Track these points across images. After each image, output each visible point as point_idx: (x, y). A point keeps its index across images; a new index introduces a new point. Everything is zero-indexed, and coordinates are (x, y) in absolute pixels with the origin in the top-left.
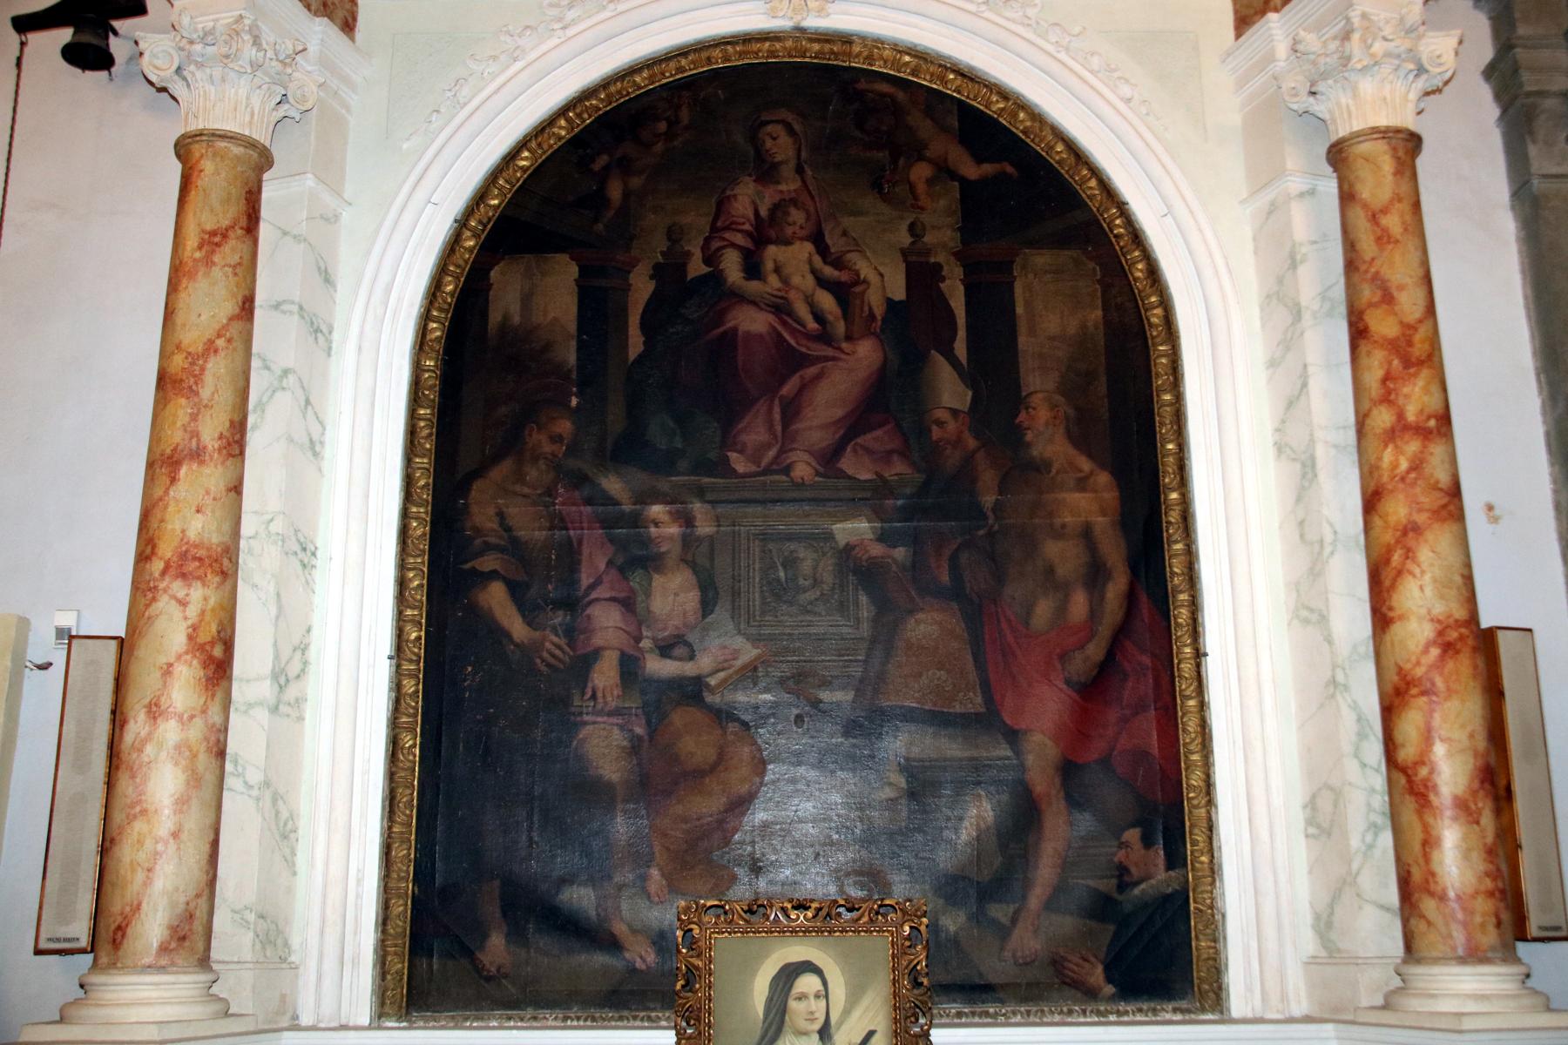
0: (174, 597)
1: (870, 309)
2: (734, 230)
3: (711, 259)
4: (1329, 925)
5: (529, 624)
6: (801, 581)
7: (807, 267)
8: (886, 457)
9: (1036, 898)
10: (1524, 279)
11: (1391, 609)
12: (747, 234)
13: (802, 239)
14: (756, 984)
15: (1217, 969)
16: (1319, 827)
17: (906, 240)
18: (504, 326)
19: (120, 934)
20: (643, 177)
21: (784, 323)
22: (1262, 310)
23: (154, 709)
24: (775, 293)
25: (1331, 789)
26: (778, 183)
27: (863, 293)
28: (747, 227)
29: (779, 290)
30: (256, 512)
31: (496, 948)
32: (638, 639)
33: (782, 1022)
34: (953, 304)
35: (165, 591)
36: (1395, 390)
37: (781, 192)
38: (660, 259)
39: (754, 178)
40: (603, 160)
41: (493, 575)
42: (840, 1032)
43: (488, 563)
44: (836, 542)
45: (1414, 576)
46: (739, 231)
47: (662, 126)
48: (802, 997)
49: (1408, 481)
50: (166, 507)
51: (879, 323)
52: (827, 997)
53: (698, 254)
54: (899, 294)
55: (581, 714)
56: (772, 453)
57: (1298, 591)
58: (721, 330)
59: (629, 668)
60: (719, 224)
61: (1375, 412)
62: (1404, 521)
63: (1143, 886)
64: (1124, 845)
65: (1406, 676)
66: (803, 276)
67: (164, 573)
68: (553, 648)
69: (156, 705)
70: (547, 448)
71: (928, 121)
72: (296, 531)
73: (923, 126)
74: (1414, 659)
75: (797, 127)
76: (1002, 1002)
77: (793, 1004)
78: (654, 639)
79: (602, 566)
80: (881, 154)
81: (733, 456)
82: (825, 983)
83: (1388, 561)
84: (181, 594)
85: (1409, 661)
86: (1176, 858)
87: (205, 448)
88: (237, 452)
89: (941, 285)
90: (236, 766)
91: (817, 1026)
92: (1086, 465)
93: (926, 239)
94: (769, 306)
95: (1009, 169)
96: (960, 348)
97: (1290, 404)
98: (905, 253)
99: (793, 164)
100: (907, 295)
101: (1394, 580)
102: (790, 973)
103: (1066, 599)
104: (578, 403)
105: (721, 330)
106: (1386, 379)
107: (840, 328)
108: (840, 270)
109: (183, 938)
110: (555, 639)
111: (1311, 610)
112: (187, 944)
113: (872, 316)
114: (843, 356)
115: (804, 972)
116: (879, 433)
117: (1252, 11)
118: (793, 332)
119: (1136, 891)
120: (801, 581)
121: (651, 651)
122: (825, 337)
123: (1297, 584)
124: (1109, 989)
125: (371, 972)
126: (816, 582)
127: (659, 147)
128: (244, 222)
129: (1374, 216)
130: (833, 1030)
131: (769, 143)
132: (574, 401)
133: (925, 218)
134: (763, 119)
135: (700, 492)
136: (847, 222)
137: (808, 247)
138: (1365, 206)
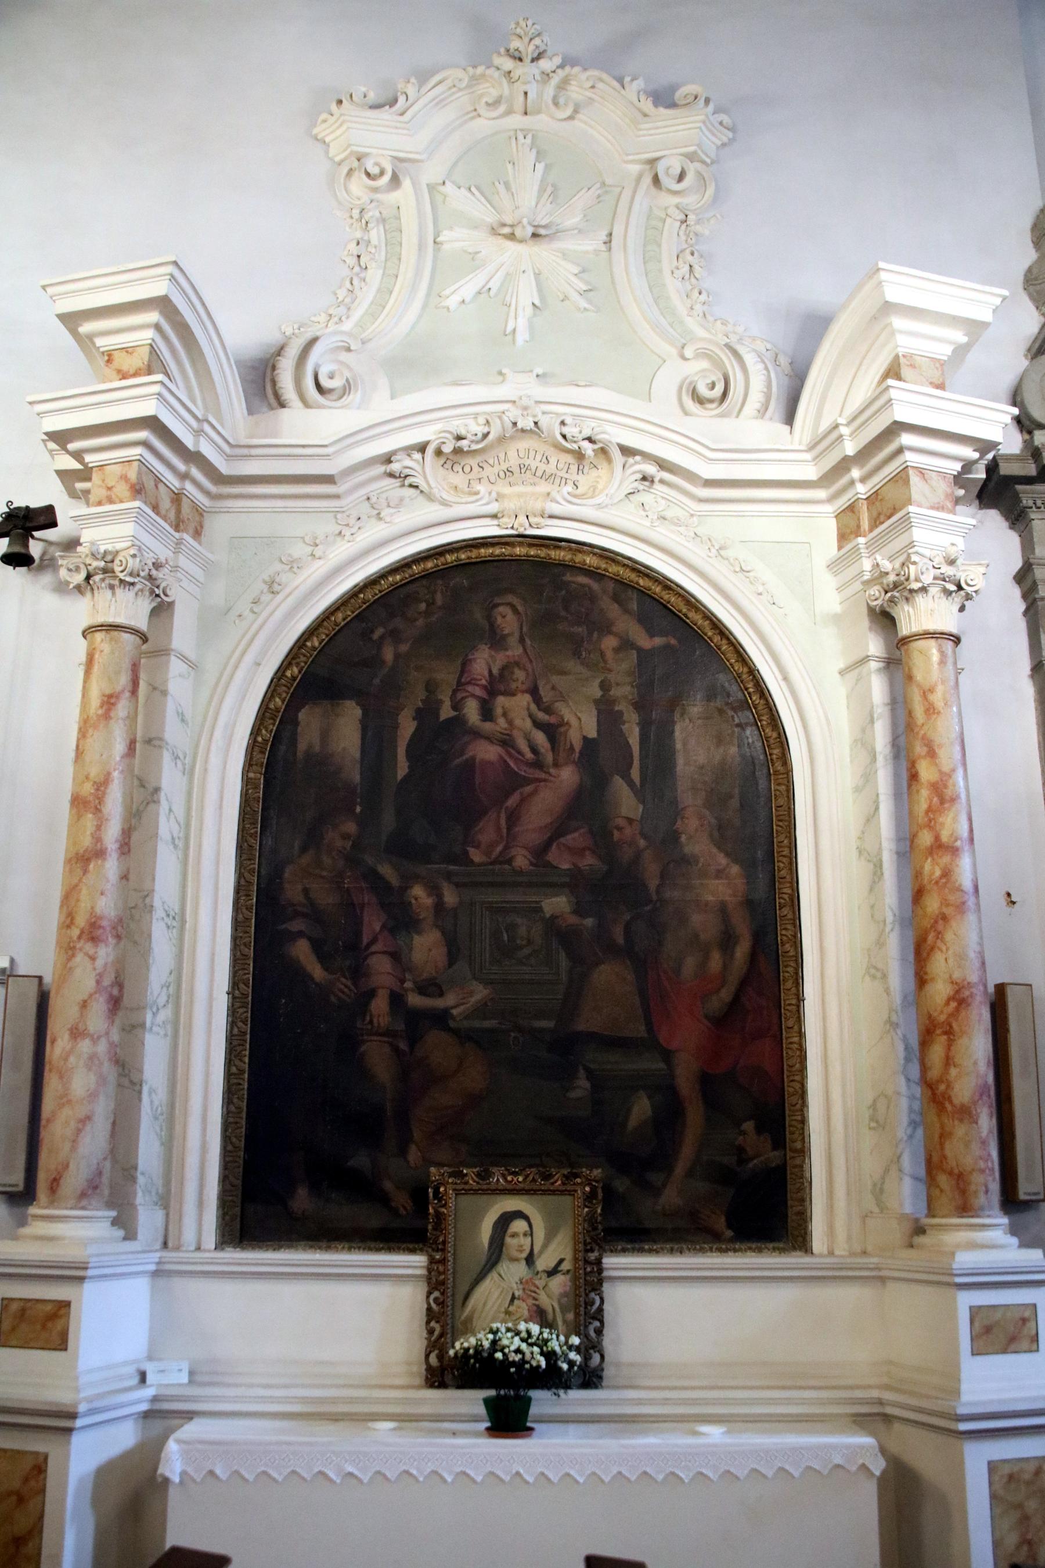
0: (86, 954)
1: (572, 745)
2: (475, 684)
3: (456, 706)
4: (882, 1191)
5: (326, 969)
6: (518, 942)
7: (526, 713)
8: (580, 852)
9: (680, 1168)
10: (1038, 729)
11: (926, 973)
12: (485, 687)
13: (523, 692)
14: (483, 1225)
15: (804, 1219)
16: (877, 1122)
17: (598, 693)
18: (309, 755)
19: (55, 1184)
20: (408, 645)
21: (510, 755)
22: (851, 750)
23: (75, 1031)
24: (503, 731)
25: (886, 1096)
26: (506, 650)
27: (567, 730)
28: (484, 682)
29: (506, 729)
30: (135, 890)
31: (302, 1200)
32: (402, 981)
33: (501, 1251)
34: (631, 741)
35: (81, 949)
36: (934, 819)
37: (508, 656)
38: (420, 704)
39: (489, 646)
40: (379, 632)
41: (301, 934)
42: (540, 1260)
43: (297, 925)
44: (544, 913)
45: (942, 951)
46: (478, 685)
47: (423, 606)
48: (514, 1235)
49: (940, 884)
50: (80, 891)
51: (577, 755)
52: (532, 1235)
53: (447, 703)
54: (593, 734)
55: (362, 1035)
56: (499, 849)
57: (869, 955)
58: (464, 758)
59: (396, 1000)
60: (463, 680)
61: (920, 834)
62: (937, 912)
63: (755, 1161)
64: (744, 1133)
65: (933, 1021)
66: (523, 719)
67: (79, 937)
68: (342, 987)
69: (76, 1029)
70: (339, 843)
71: (616, 605)
72: (163, 903)
73: (613, 610)
74: (939, 1009)
75: (520, 608)
76: (655, 1242)
77: (508, 1240)
78: (415, 982)
79: (378, 928)
80: (580, 629)
81: (472, 851)
82: (530, 1226)
83: (925, 940)
84: (91, 952)
85: (936, 1010)
86: (779, 1142)
87: (106, 849)
88: (127, 850)
89: (623, 727)
90: (123, 1069)
91: (524, 1255)
92: (722, 860)
93: (612, 693)
94: (499, 741)
95: (673, 641)
96: (635, 774)
97: (868, 820)
98: (597, 702)
99: (517, 635)
100: (598, 731)
101: (929, 954)
102: (505, 1220)
103: (706, 957)
104: (361, 811)
105: (464, 758)
106: (929, 810)
107: (549, 758)
108: (550, 715)
109: (96, 1188)
110: (343, 980)
111: (877, 969)
112: (98, 1191)
113: (572, 748)
114: (552, 779)
115: (516, 1218)
116: (576, 835)
117: (848, 531)
118: (516, 760)
119: (751, 1165)
120: (518, 942)
121: (413, 990)
122: (538, 764)
123: (869, 950)
124: (729, 1233)
125: (215, 1212)
126: (530, 942)
127: (420, 622)
128: (130, 687)
129: (924, 693)
130: (535, 1257)
131: (499, 620)
132: (358, 809)
133: (612, 677)
134: (495, 602)
135: (449, 876)
136: (555, 679)
137: (527, 697)
138: (919, 686)
